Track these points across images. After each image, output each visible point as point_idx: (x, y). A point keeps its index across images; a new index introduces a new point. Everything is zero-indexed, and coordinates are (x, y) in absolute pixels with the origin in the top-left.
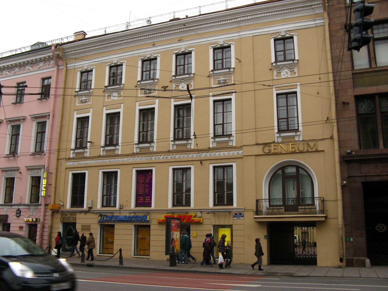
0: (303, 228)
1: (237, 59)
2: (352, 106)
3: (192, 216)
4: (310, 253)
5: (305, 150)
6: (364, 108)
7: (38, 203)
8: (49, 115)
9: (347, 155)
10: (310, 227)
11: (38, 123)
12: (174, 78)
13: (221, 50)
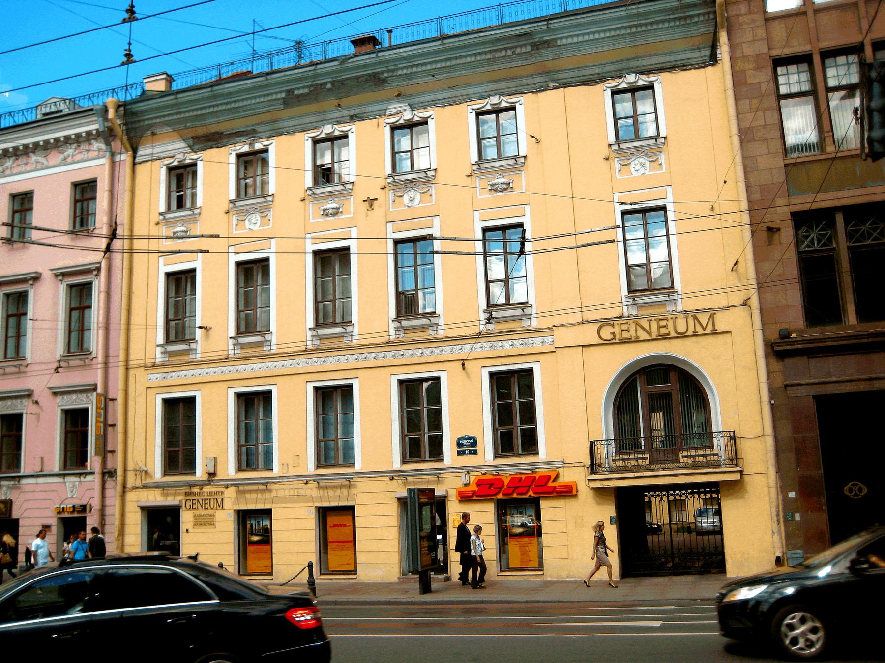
1: (533, 137)
2: (787, 233)
3: (549, 477)
6: (813, 239)
7: (85, 470)
8: (99, 269)
9: (779, 341)
11: (71, 287)
12: (390, 180)
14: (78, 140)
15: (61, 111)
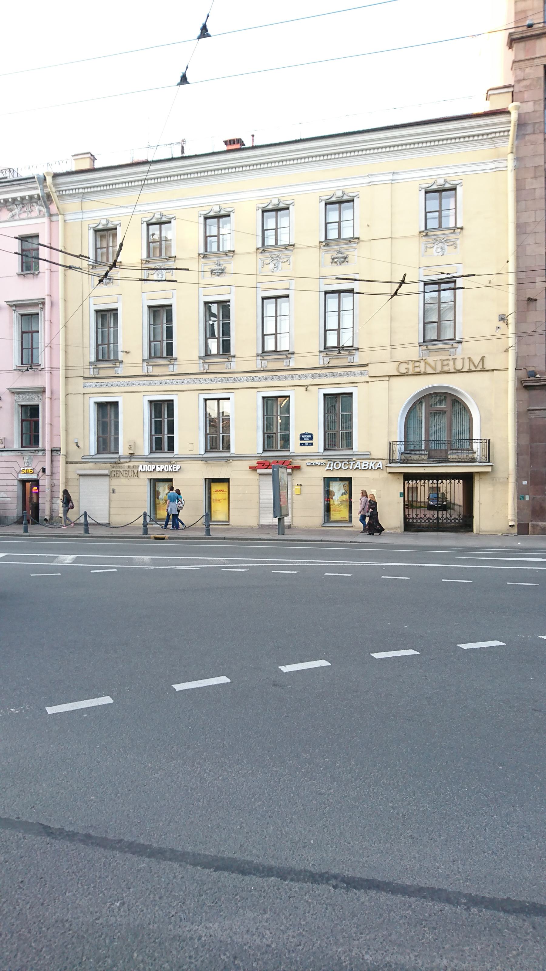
0: (410, 482)
4: (419, 516)
5: (465, 369)
8: (44, 304)
9: (528, 379)
10: (420, 481)
13: (274, 213)
14: (22, 202)
15: (6, 178)
